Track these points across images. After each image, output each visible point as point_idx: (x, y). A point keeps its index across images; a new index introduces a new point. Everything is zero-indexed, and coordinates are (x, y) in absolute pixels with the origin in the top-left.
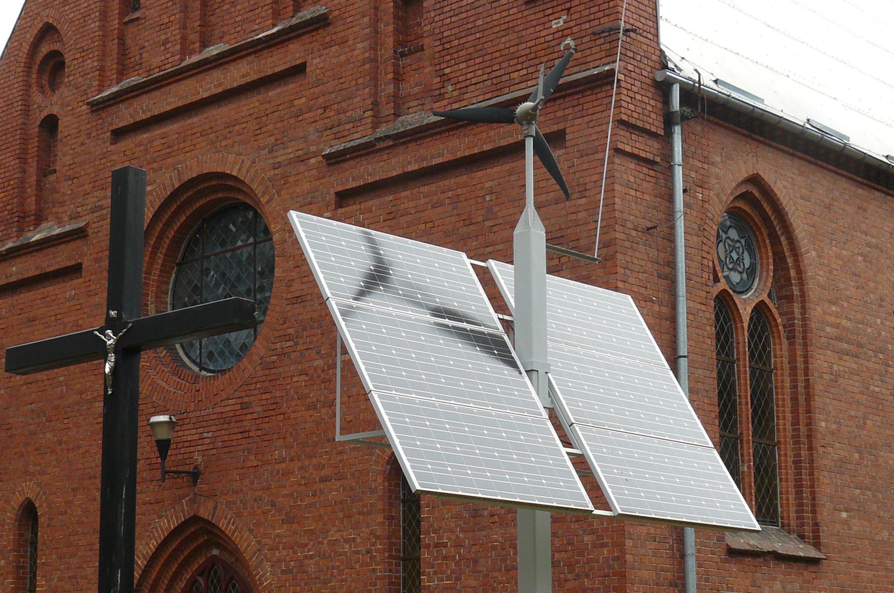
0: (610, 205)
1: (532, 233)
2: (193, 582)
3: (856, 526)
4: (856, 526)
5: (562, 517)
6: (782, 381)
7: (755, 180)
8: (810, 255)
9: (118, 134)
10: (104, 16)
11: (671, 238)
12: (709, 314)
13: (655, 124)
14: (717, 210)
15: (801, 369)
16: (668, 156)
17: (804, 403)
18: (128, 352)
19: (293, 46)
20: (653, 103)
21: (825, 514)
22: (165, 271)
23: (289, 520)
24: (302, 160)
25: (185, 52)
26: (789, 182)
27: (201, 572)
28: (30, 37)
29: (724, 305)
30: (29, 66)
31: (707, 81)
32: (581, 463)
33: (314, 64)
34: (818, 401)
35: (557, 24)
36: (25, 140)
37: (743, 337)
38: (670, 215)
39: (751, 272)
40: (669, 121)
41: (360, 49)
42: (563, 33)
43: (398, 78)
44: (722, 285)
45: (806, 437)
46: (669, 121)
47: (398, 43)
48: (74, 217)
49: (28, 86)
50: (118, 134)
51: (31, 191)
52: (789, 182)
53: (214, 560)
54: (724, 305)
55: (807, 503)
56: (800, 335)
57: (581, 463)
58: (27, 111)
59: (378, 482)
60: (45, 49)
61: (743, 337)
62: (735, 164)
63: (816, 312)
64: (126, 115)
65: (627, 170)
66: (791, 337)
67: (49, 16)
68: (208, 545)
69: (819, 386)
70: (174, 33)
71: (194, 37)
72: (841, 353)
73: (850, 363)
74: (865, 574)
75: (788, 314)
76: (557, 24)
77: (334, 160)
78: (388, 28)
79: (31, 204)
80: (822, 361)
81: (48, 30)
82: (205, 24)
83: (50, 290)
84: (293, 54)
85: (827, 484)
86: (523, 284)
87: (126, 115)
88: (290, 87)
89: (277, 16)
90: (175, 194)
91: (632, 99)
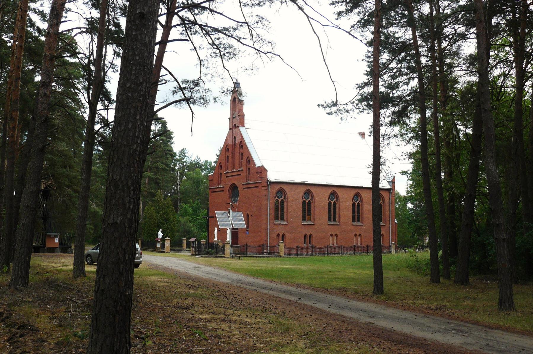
6: (285, 207)
17: (287, 209)
21: (289, 219)
55: (287, 219)
64: (227, 175)
65: (263, 191)
67: (221, 161)
80: (289, 204)
85: (289, 216)
87: (227, 175)
91: (265, 184)
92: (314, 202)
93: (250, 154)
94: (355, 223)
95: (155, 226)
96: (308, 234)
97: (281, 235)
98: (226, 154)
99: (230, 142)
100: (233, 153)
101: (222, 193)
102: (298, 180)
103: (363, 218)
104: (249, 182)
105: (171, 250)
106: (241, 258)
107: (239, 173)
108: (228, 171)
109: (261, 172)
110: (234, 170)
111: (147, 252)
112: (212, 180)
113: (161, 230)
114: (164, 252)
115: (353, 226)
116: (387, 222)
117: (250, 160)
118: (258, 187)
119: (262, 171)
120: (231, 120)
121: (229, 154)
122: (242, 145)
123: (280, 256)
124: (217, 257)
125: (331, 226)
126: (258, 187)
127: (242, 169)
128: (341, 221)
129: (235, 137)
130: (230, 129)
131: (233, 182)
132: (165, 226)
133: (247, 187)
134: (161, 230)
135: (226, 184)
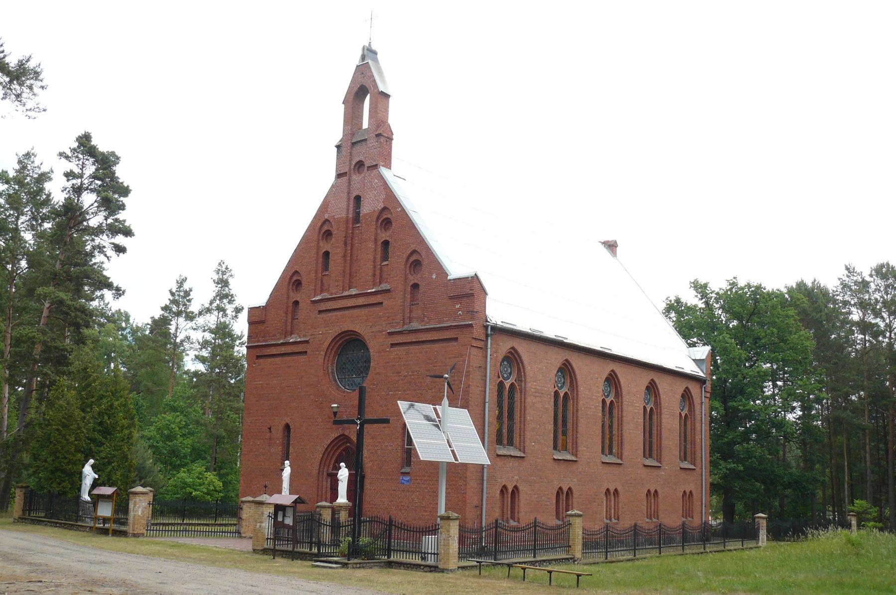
0: (469, 361)
1: (446, 401)
2: (341, 453)
3: (537, 447)
4: (537, 447)
5: (449, 464)
6: (517, 405)
7: (513, 348)
8: (528, 368)
9: (320, 312)
10: (316, 272)
11: (486, 368)
12: (496, 388)
13: (483, 337)
14: (500, 358)
15: (523, 402)
16: (486, 346)
17: (523, 411)
18: (362, 425)
19: (379, 296)
20: (482, 331)
21: (527, 443)
22: (334, 357)
23: (372, 438)
24: (381, 332)
25: (344, 290)
26: (523, 348)
27: (344, 450)
28: (290, 274)
29: (501, 385)
30: (289, 283)
31: (499, 323)
32: (453, 451)
33: (385, 303)
34: (527, 411)
35: (458, 306)
36: (287, 307)
37: (506, 393)
38: (486, 362)
39: (510, 374)
40: (487, 336)
41: (400, 302)
42: (459, 310)
43: (411, 312)
44: (501, 379)
45: (523, 422)
46: (487, 336)
47: (411, 301)
48: (305, 336)
49: (288, 289)
50: (320, 312)
51: (289, 324)
52: (523, 348)
53: (347, 448)
54: (501, 385)
55: (523, 441)
56: (523, 392)
57: (453, 451)
58: (288, 298)
59: (400, 430)
60: (295, 278)
61: (506, 393)
62: (505, 345)
63: (529, 385)
64: (323, 306)
65: (474, 351)
66: (521, 392)
67: (297, 268)
68: (346, 442)
69: (528, 407)
70: (341, 283)
71: (346, 285)
72: (536, 397)
73: (538, 399)
74: (539, 461)
75: (520, 386)
76: (458, 306)
77: (391, 334)
78: (408, 296)
79: (289, 328)
80: (529, 400)
81: (296, 272)
82: (350, 282)
83: (295, 357)
84: (379, 298)
85: (528, 434)
86: (443, 412)
87: (323, 306)
88: (377, 309)
89: (374, 285)
90: (339, 334)
91: (478, 332)
92: (576, 399)
93: (422, 241)
94: (648, 462)
95: (78, 450)
96: (565, 489)
97: (510, 490)
98: (318, 247)
99: (341, 211)
100: (349, 242)
101: (302, 358)
102: (550, 333)
103: (660, 447)
104: (415, 325)
105: (152, 527)
106: (517, 571)
107: (373, 300)
108: (326, 295)
109: (472, 295)
110: (353, 292)
111: (50, 530)
112: (263, 322)
113: (92, 461)
114: (124, 534)
115: (645, 470)
116: (698, 461)
117: (420, 258)
118: (456, 339)
119: (470, 291)
120: (346, 150)
121: (335, 247)
122: (392, 218)
123: (574, 560)
124: (390, 565)
125: (607, 468)
126: (456, 339)
127: (385, 286)
128: (626, 453)
129: (358, 199)
130: (339, 176)
131: (348, 326)
132: (106, 450)
133: (403, 339)
134: (92, 461)
135: (322, 332)
